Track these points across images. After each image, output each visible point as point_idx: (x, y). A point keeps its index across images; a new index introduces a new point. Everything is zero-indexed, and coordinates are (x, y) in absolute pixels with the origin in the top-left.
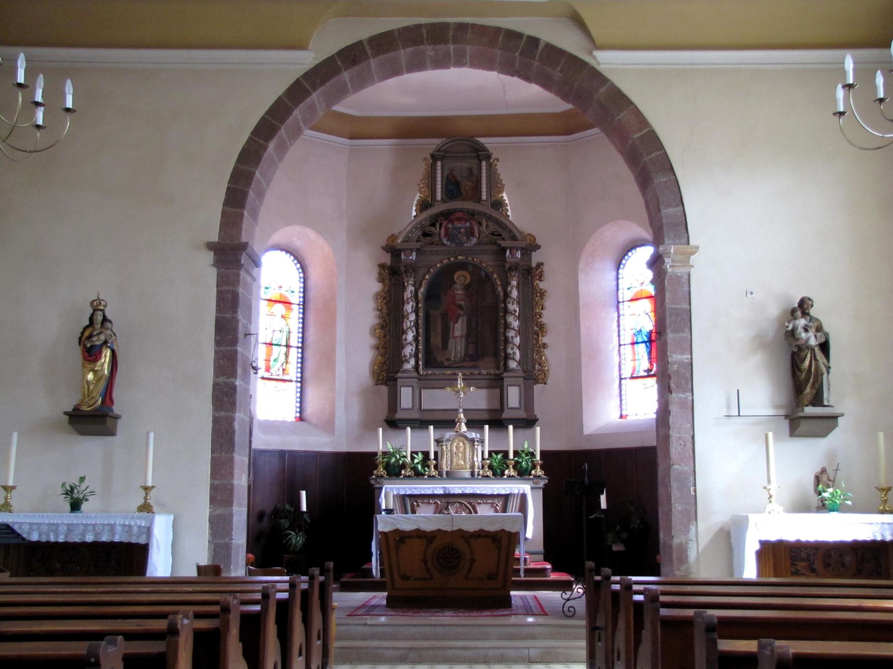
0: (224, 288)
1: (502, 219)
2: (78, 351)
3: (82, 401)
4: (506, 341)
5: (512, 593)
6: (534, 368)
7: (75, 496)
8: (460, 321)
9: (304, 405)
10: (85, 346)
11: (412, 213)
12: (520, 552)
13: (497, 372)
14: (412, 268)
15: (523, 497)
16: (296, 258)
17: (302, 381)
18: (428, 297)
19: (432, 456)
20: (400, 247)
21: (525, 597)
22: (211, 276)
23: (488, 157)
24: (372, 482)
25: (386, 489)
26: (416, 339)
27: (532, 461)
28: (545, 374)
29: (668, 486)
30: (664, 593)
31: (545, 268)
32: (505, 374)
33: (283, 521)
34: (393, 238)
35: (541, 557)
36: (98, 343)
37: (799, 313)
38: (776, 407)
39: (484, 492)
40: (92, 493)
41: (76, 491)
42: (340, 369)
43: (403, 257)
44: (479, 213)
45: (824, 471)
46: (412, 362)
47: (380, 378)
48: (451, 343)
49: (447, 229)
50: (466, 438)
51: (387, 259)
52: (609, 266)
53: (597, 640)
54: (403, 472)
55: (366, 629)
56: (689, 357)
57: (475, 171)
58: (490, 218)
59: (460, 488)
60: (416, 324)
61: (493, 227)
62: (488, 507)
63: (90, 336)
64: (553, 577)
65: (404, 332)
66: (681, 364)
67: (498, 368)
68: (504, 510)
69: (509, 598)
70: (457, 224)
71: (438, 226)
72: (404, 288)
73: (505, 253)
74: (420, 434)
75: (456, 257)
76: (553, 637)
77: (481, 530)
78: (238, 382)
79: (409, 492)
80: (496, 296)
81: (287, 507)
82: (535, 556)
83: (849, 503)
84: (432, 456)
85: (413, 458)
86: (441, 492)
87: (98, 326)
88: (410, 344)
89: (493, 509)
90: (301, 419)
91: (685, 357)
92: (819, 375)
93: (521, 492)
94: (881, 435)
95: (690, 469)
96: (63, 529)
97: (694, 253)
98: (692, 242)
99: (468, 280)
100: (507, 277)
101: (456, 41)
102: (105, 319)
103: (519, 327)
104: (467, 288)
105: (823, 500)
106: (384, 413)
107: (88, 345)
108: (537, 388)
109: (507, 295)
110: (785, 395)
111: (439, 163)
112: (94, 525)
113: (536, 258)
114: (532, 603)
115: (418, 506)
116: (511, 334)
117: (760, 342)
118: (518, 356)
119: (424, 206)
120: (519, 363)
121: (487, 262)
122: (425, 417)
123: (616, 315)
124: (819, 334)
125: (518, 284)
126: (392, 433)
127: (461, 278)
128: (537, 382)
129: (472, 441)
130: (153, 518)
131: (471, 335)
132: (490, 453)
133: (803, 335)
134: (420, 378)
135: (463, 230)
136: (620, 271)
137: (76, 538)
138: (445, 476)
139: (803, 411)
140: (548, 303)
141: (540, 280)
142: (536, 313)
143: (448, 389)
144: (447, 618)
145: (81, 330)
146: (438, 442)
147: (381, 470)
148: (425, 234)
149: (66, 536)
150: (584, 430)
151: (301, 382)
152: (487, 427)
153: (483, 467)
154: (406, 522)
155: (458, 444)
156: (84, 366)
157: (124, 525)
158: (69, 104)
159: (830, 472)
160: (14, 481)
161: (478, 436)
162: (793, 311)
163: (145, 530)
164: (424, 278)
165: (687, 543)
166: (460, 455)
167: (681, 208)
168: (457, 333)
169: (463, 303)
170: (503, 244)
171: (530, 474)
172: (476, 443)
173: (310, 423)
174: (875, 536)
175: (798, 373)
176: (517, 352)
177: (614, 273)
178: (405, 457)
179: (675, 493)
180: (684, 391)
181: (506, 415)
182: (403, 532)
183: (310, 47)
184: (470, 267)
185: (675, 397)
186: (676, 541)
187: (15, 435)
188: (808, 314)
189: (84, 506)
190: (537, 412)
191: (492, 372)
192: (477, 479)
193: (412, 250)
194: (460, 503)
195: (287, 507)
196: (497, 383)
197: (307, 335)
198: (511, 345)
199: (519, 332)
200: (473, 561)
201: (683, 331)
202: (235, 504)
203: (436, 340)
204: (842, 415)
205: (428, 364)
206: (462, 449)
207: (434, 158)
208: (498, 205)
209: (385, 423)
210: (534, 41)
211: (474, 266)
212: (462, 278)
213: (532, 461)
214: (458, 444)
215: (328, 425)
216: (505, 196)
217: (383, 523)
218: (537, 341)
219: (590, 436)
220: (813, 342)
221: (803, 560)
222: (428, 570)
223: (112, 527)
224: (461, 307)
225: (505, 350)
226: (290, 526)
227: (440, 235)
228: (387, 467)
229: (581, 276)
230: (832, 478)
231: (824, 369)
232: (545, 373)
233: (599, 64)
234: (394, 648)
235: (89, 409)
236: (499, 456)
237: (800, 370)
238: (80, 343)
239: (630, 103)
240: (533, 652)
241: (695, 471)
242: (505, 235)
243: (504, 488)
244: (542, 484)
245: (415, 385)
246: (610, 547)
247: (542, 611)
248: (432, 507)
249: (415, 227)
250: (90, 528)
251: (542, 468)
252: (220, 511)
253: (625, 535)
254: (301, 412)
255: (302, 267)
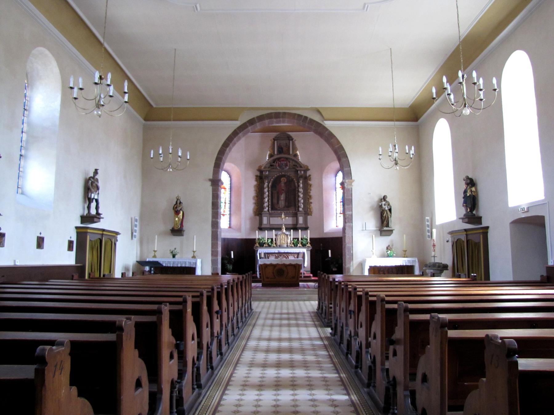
0: (214, 192)
1: (297, 161)
2: (172, 212)
3: (174, 226)
4: (298, 201)
5: (300, 283)
6: (308, 210)
7: (174, 253)
8: (283, 194)
9: (231, 223)
10: (175, 210)
11: (266, 158)
12: (302, 271)
13: (295, 212)
14: (267, 177)
15: (304, 253)
16: (228, 173)
17: (230, 214)
18: (272, 187)
19: (274, 240)
20: (263, 170)
21: (304, 284)
22: (210, 189)
23: (292, 139)
24: (255, 248)
25: (259, 251)
26: (268, 201)
27: (307, 242)
28: (311, 212)
29: (345, 250)
30: (387, 296)
31: (311, 177)
32: (298, 213)
33: (225, 261)
34: (260, 167)
35: (310, 272)
36: (179, 209)
37: (383, 200)
38: (376, 227)
39: (291, 252)
40: (178, 253)
41: (174, 252)
42: (243, 210)
43: (264, 173)
44: (289, 158)
45: (389, 246)
46: (267, 208)
47: (257, 213)
48: (280, 202)
49: (278, 164)
50: (285, 234)
51: (258, 174)
52: (333, 176)
53: (336, 306)
54: (265, 245)
55: (257, 292)
56: (351, 213)
57: (288, 144)
58: (293, 160)
59: (283, 250)
60: (268, 196)
61: (294, 163)
62: (292, 256)
63: (176, 208)
64: (313, 278)
65: (264, 198)
66: (349, 215)
67: (296, 210)
68: (298, 257)
69: (299, 284)
70: (282, 162)
71: (275, 162)
72: (264, 184)
73: (298, 172)
74: (270, 232)
75: (281, 173)
76: (310, 294)
77: (290, 264)
78: (219, 221)
79: (267, 252)
80: (295, 186)
81: (226, 256)
82: (307, 272)
83: (395, 255)
84: (274, 240)
85: (268, 241)
86: (277, 252)
87: (178, 204)
88: (266, 202)
89: (294, 257)
90: (230, 227)
91: (350, 213)
92: (388, 218)
93: (303, 252)
94: (405, 236)
95: (351, 246)
96: (172, 263)
97: (353, 182)
98: (353, 178)
99: (286, 181)
100: (298, 180)
101: (283, 117)
102: (180, 203)
103: (303, 197)
104: (285, 183)
105: (388, 254)
106: (257, 226)
107: (176, 210)
108: (309, 217)
109: (299, 186)
110: (379, 224)
111: (276, 142)
112: (180, 262)
113: (308, 173)
114: (305, 285)
115: (270, 256)
116: (300, 199)
117: (372, 208)
118: (302, 206)
119: (271, 156)
120: (303, 209)
121: (292, 174)
122: (272, 227)
123: (335, 192)
124: (388, 206)
125: (302, 182)
126: (261, 232)
127: (283, 180)
128: (308, 215)
129: (287, 235)
130: (197, 260)
131: (286, 199)
132: (293, 239)
133: (384, 207)
134: (270, 214)
135: (284, 164)
136: (336, 177)
137: (175, 265)
138: (278, 246)
139: (383, 229)
140: (312, 188)
141: (310, 180)
142: (309, 192)
143: (279, 218)
144: (281, 289)
145: (174, 205)
146: (276, 235)
147: (257, 245)
148: (271, 166)
149: (173, 265)
150: (325, 228)
151: (230, 215)
152: (292, 230)
153: (291, 243)
154: (267, 261)
155: (283, 236)
156: (175, 216)
157: (189, 262)
158: (188, 158)
159: (391, 246)
160: (157, 249)
161: (289, 233)
162: (381, 200)
163: (195, 263)
164: (271, 180)
165: (350, 267)
166: (283, 239)
167: (350, 168)
168: (282, 199)
169: (284, 188)
170: (298, 169)
171: (306, 246)
172: (288, 236)
173: (233, 229)
174: (403, 264)
175: (382, 218)
176: (302, 205)
177: (335, 178)
178: (265, 240)
179: (347, 253)
180: (350, 223)
181: (298, 226)
182: (267, 264)
183: (239, 119)
184: (286, 176)
185: (347, 224)
186: (347, 266)
187: (156, 236)
188: (386, 200)
189: (176, 256)
190: (309, 225)
191: (294, 212)
192: (289, 247)
193: (267, 171)
194: (283, 255)
195: (226, 256)
196: (295, 215)
197: (232, 199)
198: (300, 203)
199: (303, 198)
200: (288, 273)
201: (350, 205)
202: (218, 256)
203: (275, 201)
204: (394, 230)
205: (272, 209)
206: (284, 238)
207: (274, 140)
208: (296, 155)
209: (258, 229)
210: (306, 118)
211: (288, 176)
212: (284, 180)
213: (307, 242)
214: (283, 236)
215: (239, 230)
216: (298, 152)
217: (260, 262)
218: (309, 201)
219: (326, 233)
220: (387, 209)
221: (382, 271)
222: (274, 276)
223: (185, 262)
224: (283, 190)
225: (298, 204)
226: (228, 262)
227: (276, 165)
228: (259, 244)
229: (323, 179)
230: (391, 248)
231: (390, 217)
232: (311, 212)
233: (325, 124)
234: (265, 297)
235: (177, 229)
236: (296, 240)
237: (383, 217)
238: (173, 209)
239: (335, 136)
240: (305, 298)
241: (352, 246)
242: (298, 166)
243: (298, 251)
244: (310, 249)
245: (268, 216)
246: (332, 269)
247: (308, 287)
248: (274, 257)
249: (268, 163)
250: (179, 263)
251: (310, 244)
252: (214, 258)
253: (337, 265)
254: (230, 225)
255: (230, 176)
